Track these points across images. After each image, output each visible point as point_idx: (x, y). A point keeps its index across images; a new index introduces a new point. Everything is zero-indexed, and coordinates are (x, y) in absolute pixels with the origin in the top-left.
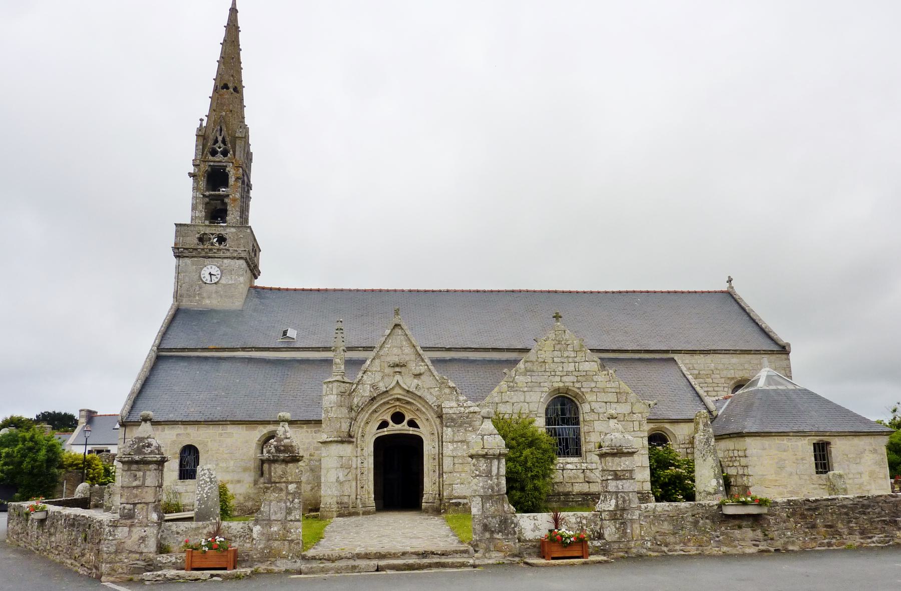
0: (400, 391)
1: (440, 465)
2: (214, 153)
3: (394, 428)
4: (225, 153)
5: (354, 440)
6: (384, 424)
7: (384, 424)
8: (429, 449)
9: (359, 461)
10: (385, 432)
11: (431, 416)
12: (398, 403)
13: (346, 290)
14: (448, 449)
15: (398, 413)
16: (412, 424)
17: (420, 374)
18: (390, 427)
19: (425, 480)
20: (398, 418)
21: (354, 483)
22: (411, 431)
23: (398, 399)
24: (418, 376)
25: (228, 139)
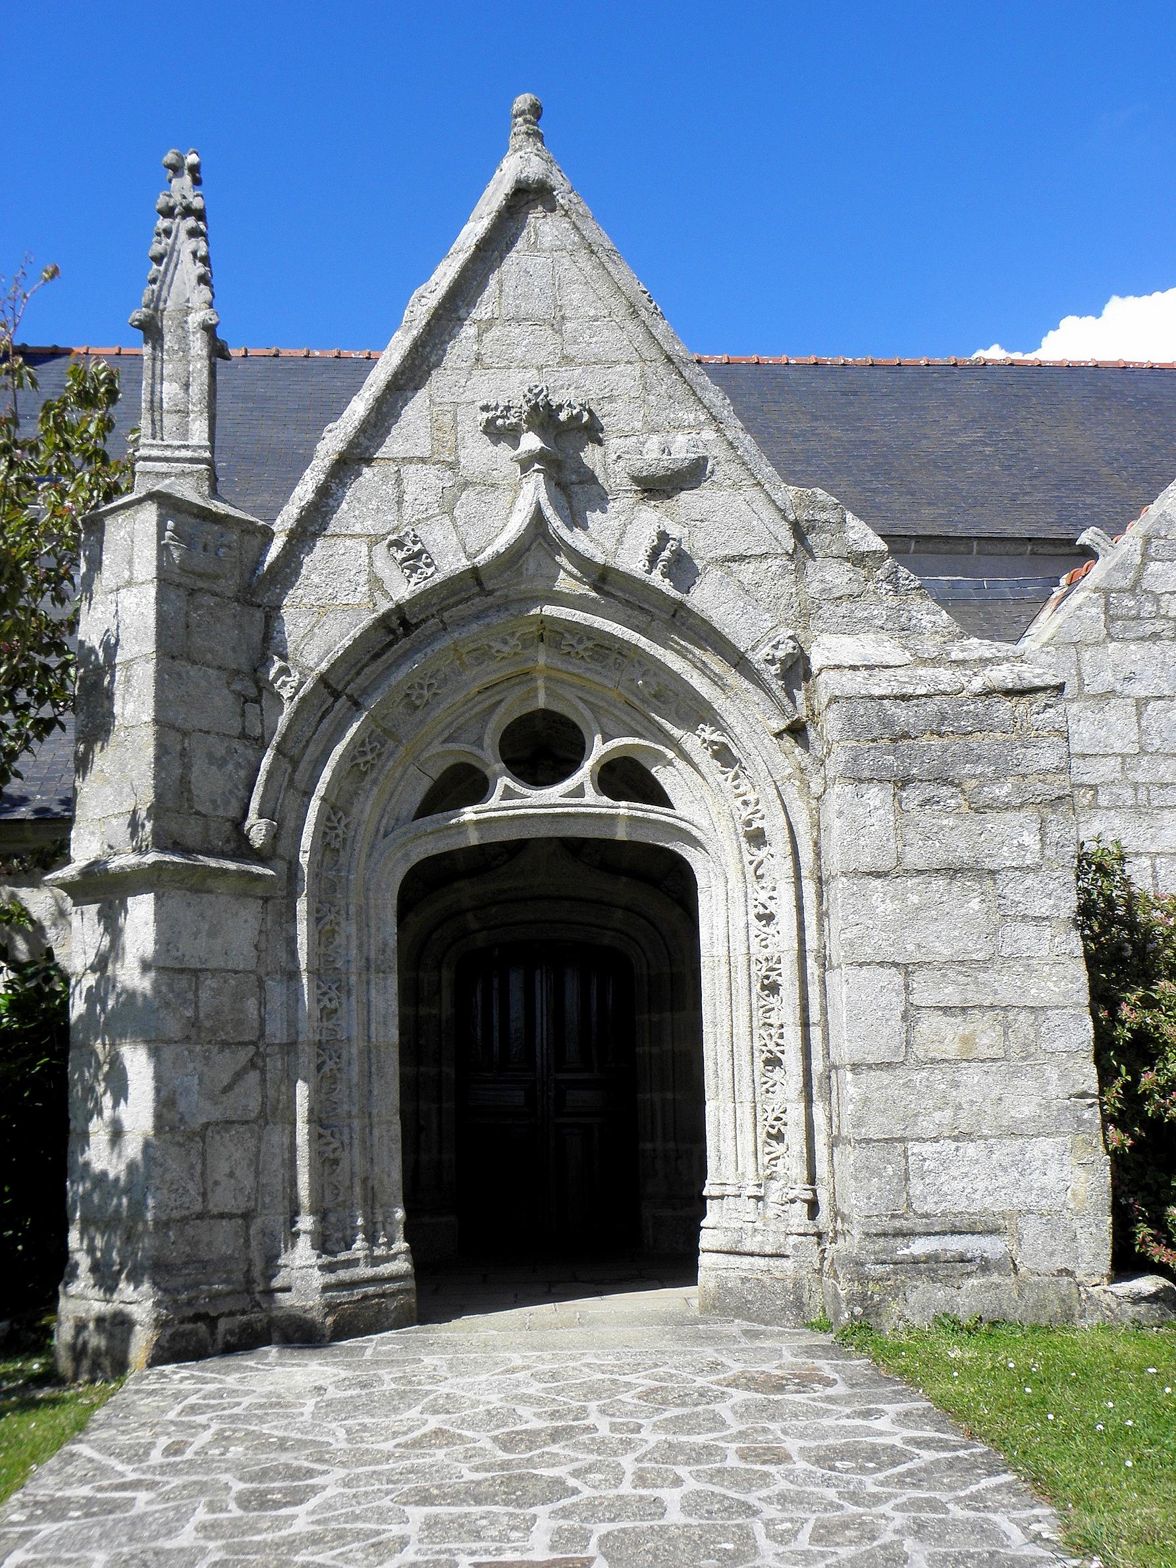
17: (691, 475)
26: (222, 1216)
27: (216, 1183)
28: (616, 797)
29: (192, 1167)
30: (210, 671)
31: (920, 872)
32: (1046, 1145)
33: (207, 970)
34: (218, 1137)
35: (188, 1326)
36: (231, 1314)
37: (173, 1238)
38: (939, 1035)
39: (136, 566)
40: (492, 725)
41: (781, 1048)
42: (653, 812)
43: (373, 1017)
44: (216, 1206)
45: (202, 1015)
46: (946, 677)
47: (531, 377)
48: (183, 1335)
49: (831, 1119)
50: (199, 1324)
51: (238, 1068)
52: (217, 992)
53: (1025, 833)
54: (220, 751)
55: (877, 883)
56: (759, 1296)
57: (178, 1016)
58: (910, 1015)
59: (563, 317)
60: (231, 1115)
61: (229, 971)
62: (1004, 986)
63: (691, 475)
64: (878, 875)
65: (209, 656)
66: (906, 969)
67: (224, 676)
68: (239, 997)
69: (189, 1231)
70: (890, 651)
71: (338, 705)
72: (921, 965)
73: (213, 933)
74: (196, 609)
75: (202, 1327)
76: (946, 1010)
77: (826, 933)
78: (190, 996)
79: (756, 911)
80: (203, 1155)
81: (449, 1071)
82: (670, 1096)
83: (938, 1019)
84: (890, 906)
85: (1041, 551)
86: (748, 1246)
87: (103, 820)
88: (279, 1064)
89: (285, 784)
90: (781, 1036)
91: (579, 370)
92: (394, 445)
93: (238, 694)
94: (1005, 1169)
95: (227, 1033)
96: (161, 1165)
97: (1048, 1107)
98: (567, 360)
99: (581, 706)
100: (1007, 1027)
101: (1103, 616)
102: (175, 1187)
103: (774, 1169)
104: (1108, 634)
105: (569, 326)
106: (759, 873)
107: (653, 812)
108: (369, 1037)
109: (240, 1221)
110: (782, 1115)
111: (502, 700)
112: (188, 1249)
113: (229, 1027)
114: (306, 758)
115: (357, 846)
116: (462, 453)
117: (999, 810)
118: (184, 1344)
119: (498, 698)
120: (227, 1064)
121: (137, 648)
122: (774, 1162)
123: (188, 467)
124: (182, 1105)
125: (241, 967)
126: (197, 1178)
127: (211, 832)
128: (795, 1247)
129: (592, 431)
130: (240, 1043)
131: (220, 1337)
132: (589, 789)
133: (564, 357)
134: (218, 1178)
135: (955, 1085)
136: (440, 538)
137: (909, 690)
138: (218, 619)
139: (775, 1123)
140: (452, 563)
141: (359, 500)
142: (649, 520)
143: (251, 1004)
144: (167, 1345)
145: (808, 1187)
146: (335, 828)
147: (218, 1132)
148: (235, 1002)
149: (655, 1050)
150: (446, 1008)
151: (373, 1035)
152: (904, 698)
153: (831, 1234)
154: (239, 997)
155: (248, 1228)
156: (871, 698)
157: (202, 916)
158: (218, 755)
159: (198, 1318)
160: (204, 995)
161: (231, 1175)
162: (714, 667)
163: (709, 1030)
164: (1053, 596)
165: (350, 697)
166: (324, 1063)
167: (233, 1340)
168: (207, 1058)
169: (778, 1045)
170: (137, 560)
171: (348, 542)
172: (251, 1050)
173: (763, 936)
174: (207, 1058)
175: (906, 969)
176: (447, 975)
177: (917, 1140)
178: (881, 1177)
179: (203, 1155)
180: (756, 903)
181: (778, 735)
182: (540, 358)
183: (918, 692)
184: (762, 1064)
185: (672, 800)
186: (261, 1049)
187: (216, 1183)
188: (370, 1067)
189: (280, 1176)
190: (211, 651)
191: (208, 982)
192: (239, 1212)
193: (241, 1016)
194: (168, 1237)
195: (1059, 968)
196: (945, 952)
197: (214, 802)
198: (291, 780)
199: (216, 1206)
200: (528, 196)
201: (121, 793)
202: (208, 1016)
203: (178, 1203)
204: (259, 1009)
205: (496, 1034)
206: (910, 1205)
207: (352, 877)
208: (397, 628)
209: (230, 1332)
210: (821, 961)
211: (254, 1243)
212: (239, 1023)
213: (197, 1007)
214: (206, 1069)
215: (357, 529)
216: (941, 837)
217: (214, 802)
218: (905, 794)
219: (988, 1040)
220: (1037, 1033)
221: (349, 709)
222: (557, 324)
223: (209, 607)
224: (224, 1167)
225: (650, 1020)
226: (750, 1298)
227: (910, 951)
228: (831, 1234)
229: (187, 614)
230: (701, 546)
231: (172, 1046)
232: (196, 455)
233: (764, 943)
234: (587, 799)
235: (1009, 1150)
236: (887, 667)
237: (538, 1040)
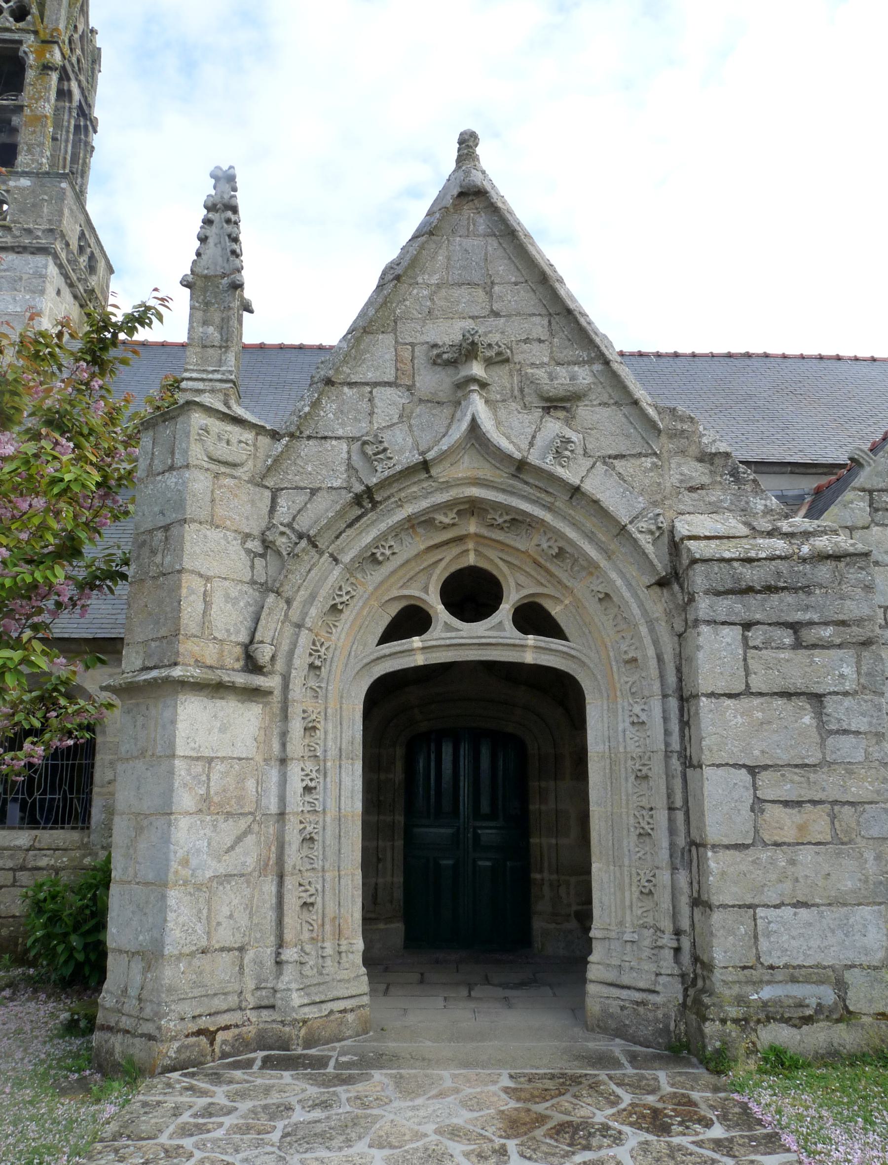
0: (486, 471)
1: (684, 807)
3: (450, 639)
5: (271, 682)
6: (410, 621)
7: (410, 621)
8: (615, 732)
9: (296, 784)
10: (415, 652)
11: (626, 581)
12: (472, 527)
13: (311, 348)
14: (722, 728)
15: (473, 571)
16: (533, 619)
18: (436, 634)
19: (600, 872)
20: (471, 595)
21: (270, 888)
22: (533, 650)
23: (473, 508)
24: (557, 404)
26: (222, 949)
27: (219, 924)
28: (526, 633)
29: (200, 911)
30: (228, 533)
31: (761, 694)
32: (865, 911)
33: (218, 758)
34: (221, 888)
35: (193, 1039)
36: (227, 1028)
37: (182, 969)
38: (783, 823)
39: (177, 456)
40: (434, 577)
41: (652, 826)
42: (552, 643)
43: (343, 793)
44: (218, 942)
45: (212, 792)
46: (779, 546)
47: (469, 324)
48: (187, 1047)
49: (691, 883)
50: (201, 1037)
51: (239, 832)
52: (226, 774)
53: (845, 665)
54: (234, 593)
55: (729, 702)
56: (635, 1021)
57: (193, 794)
58: (758, 804)
59: (492, 283)
60: (231, 870)
61: (234, 758)
62: (829, 785)
64: (730, 696)
65: (228, 523)
66: (753, 770)
67: (239, 537)
68: (241, 780)
69: (196, 962)
70: (733, 525)
71: (322, 560)
72: (766, 767)
73: (223, 729)
74: (220, 487)
75: (203, 1040)
76: (786, 804)
77: (687, 738)
78: (204, 778)
79: (631, 719)
80: (209, 902)
81: (400, 819)
82: (553, 841)
83: (778, 810)
84: (739, 719)
85: (797, 471)
86: (626, 980)
87: (145, 643)
88: (271, 830)
89: (282, 618)
90: (652, 817)
91: (503, 320)
93: (248, 551)
94: (833, 931)
95: (231, 807)
96: (175, 911)
97: (866, 881)
98: (496, 314)
99: (501, 564)
100: (833, 817)
101: (868, 509)
102: (186, 928)
103: (645, 920)
104: (873, 521)
105: (496, 288)
106: (633, 690)
107: (552, 643)
108: (340, 809)
109: (237, 953)
110: (652, 879)
111: (441, 560)
112: (194, 976)
113: (233, 802)
114: (298, 599)
115: (334, 665)
116: (417, 378)
117: (823, 647)
118: (188, 1054)
119: (440, 557)
120: (229, 830)
121: (174, 515)
122: (645, 914)
123: (219, 385)
124: (194, 862)
125: (244, 756)
126: (204, 921)
127: (225, 653)
128: (664, 985)
130: (241, 814)
131: (217, 1050)
132: (509, 625)
133: (492, 311)
134: (221, 919)
135: (792, 862)
136: (400, 440)
137: (752, 554)
138: (236, 495)
139: (646, 884)
141: (342, 412)
143: (251, 784)
144: (174, 1056)
145: (674, 937)
146: (318, 651)
147: (222, 884)
148: (238, 783)
149: (543, 808)
150: (398, 774)
151: (343, 807)
152: (749, 560)
153: (692, 976)
154: (241, 780)
155: (242, 959)
156: (723, 560)
157: (215, 716)
158: (233, 595)
159: (199, 1032)
160: (215, 777)
161: (231, 916)
162: (600, 536)
163: (386, 616)
164: (806, 501)
165: (331, 555)
166: (305, 828)
167: (227, 1049)
168: (215, 826)
169: (649, 823)
170: (177, 451)
171: (334, 442)
172: (250, 818)
173: (636, 739)
174: (215, 826)
175: (753, 770)
176: (400, 752)
177: (763, 906)
178: (734, 934)
179: (209, 902)
180: (631, 713)
181: (648, 587)
182: (476, 311)
183: (761, 556)
184: (636, 838)
185: (568, 635)
186: (257, 818)
187: (219, 924)
188: (340, 832)
189: (269, 918)
190: (230, 518)
191: (218, 767)
192: (236, 946)
193: (243, 794)
194: (179, 968)
195: (873, 771)
196: (784, 757)
197: (228, 631)
198: (286, 615)
199: (218, 942)
201: (159, 623)
202: (216, 794)
203: (188, 941)
204: (257, 788)
205: (433, 792)
206: (758, 958)
207: (330, 688)
209: (224, 1042)
210: (682, 760)
211: (247, 970)
212: (240, 799)
213: (208, 787)
214: (213, 834)
215: (340, 433)
216: (779, 667)
217: (228, 631)
218: (750, 634)
219: (820, 827)
220: (858, 823)
221: (331, 563)
222: (489, 287)
223: (228, 487)
224: (226, 911)
225: (540, 787)
226: (627, 1022)
227: (755, 757)
228: (692, 976)
229: (212, 492)
231: (188, 818)
232: (225, 377)
233: (637, 744)
234: (507, 634)
235: (837, 915)
236: (733, 537)
237: (461, 798)
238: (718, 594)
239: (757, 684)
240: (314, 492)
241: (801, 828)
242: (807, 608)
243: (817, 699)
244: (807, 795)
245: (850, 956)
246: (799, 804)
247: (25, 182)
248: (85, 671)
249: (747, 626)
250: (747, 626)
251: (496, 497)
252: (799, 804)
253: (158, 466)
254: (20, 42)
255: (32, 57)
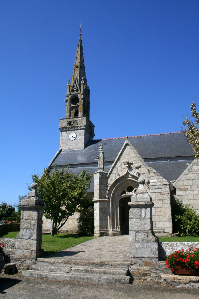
2: (73, 91)
4: (77, 90)
15: (130, 186)
17: (140, 167)
25: (78, 85)
63: (140, 167)
76: (159, 211)
92: (117, 166)
98: (130, 158)
129: (132, 163)
140: (121, 175)
142: (137, 170)
200: (127, 145)
208: (117, 181)
230: (141, 173)
238: (152, 189)
239: (156, 199)
240: (112, 179)
241: (160, 214)
242: (162, 190)
243: (162, 200)
244: (161, 210)
245: (165, 227)
246: (160, 211)
247: (80, 118)
248: (19, 197)
249: (155, 193)
250: (155, 193)
251: (96, 194)
252: (160, 211)
253: (96, 178)
254: (78, 95)
255: (80, 97)
